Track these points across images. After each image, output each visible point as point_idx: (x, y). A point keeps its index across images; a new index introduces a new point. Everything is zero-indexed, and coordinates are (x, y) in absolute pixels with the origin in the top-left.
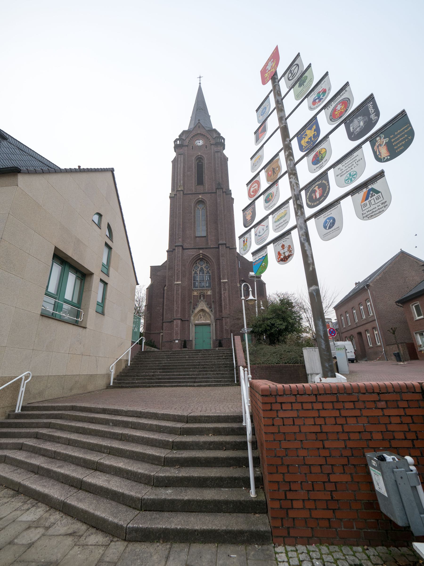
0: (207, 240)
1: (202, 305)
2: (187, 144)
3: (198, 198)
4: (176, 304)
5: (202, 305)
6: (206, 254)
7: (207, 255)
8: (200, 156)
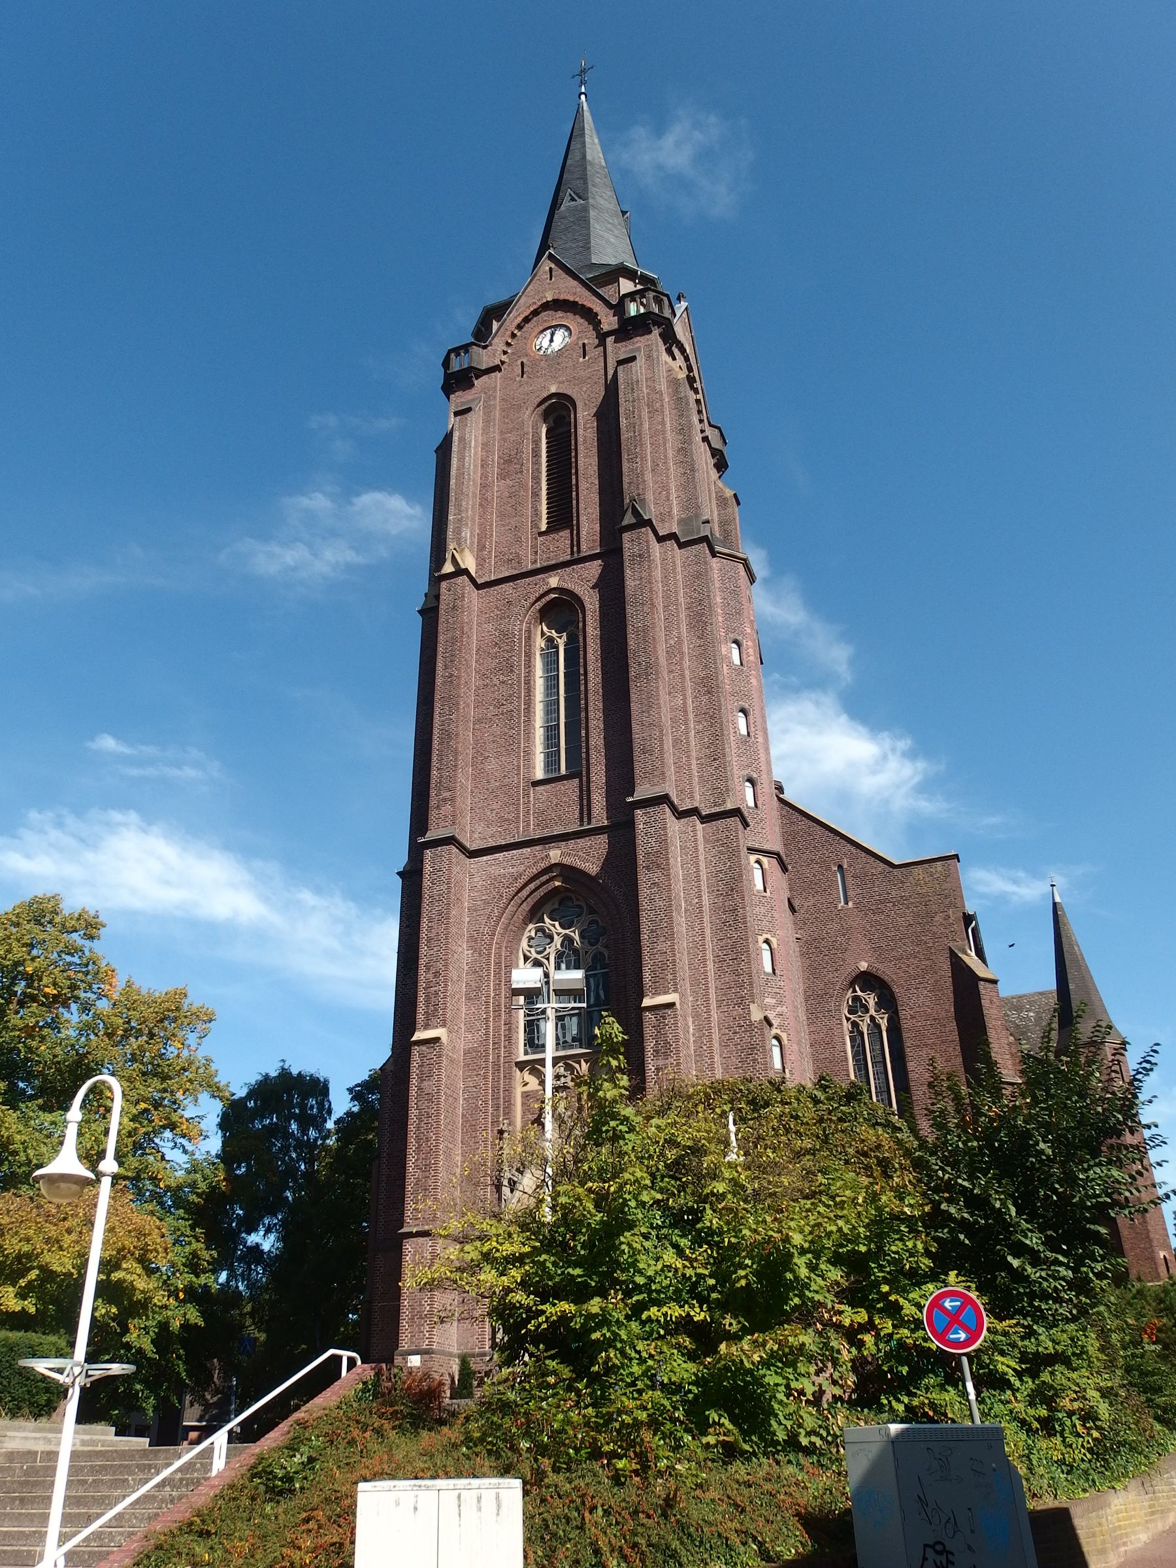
2: (497, 362)
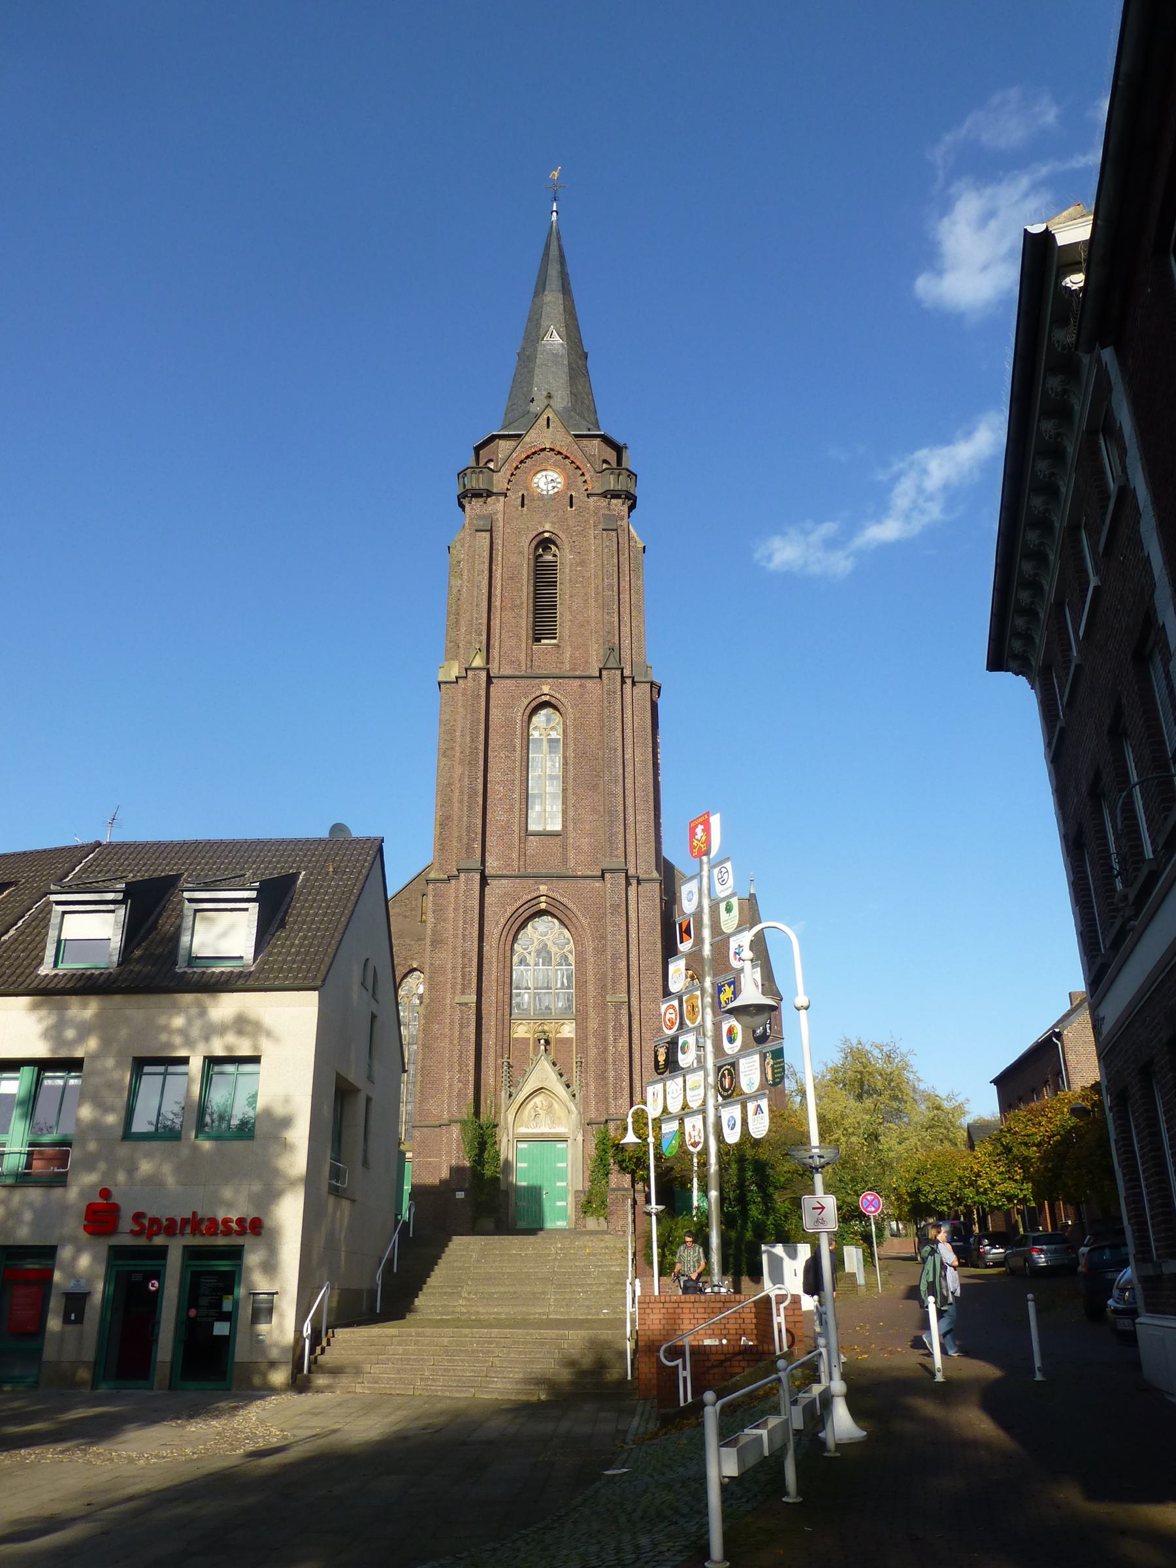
0: (564, 847)
1: (543, 1073)
3: (538, 693)
4: (460, 1071)
5: (543, 1073)
6: (559, 898)
7: (564, 900)
8: (547, 535)
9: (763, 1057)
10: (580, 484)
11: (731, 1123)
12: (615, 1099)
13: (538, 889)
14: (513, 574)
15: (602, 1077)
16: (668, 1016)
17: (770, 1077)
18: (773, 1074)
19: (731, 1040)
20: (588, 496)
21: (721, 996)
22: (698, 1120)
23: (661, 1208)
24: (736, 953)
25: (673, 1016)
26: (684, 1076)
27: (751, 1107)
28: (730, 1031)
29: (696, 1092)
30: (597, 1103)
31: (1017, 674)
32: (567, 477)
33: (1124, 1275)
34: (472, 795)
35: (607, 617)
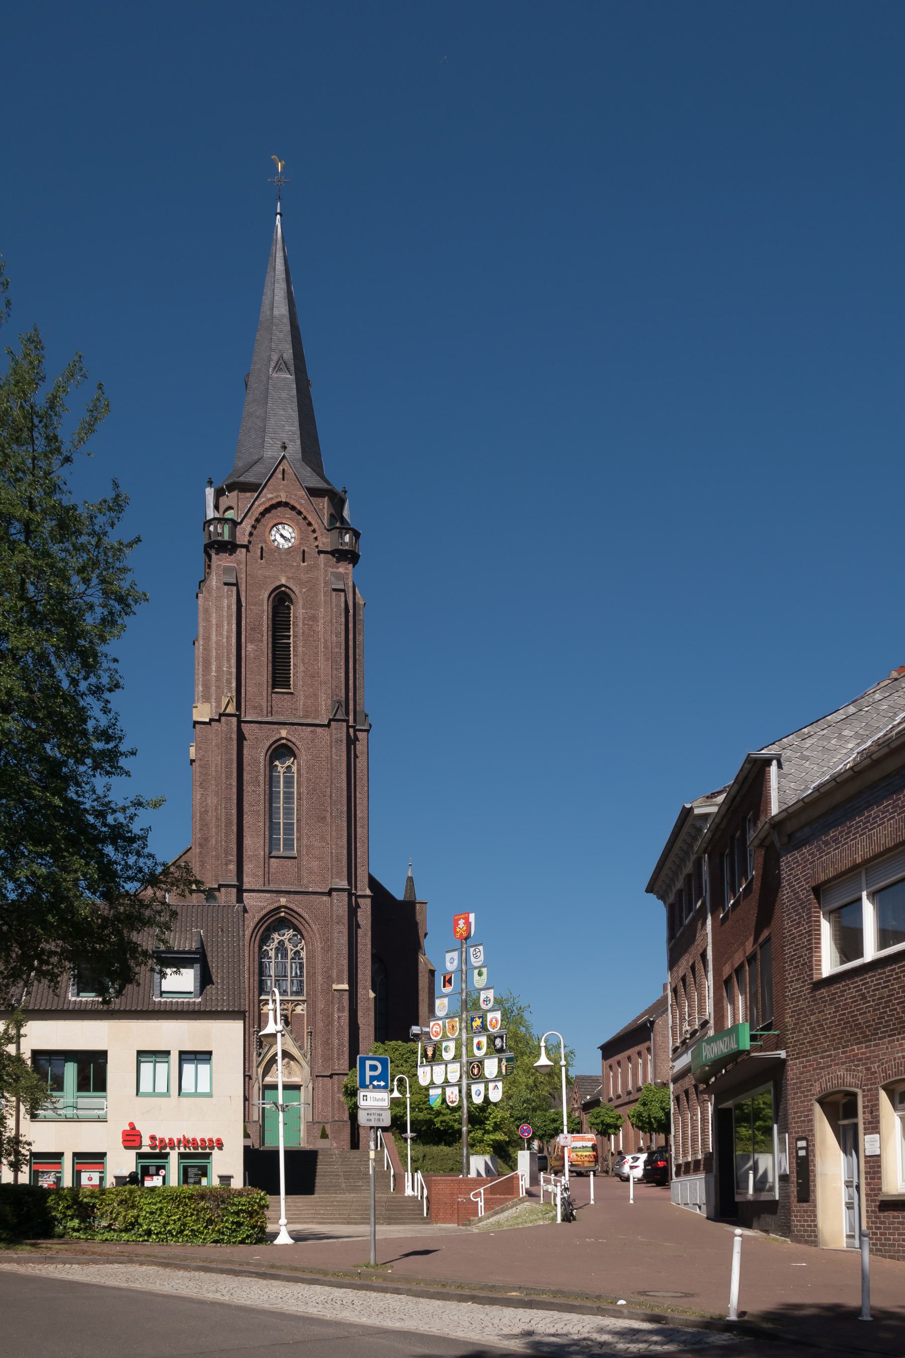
3: (277, 737)
6: (295, 908)
7: (299, 910)
9: (500, 1061)
10: (312, 539)
11: (478, 1092)
12: (339, 1059)
13: (279, 900)
14: (254, 625)
15: (327, 1043)
16: (434, 1029)
17: (504, 1071)
18: (506, 1070)
19: (479, 1048)
20: (320, 552)
21: (473, 1023)
22: (456, 1090)
23: (414, 1134)
24: (484, 1001)
25: (438, 1030)
26: (446, 1065)
27: (491, 1085)
28: (479, 1044)
29: (454, 1074)
30: (323, 1061)
31: (659, 898)
32: (301, 531)
33: (207, 649)
34: (228, 824)
35: (335, 672)
